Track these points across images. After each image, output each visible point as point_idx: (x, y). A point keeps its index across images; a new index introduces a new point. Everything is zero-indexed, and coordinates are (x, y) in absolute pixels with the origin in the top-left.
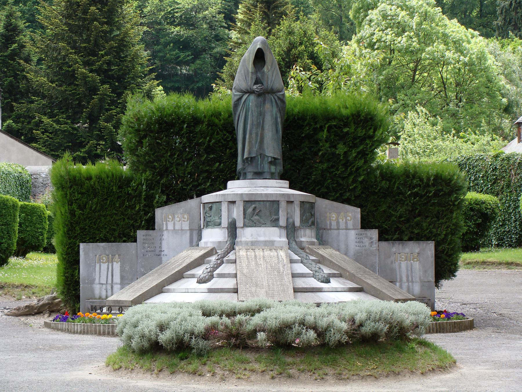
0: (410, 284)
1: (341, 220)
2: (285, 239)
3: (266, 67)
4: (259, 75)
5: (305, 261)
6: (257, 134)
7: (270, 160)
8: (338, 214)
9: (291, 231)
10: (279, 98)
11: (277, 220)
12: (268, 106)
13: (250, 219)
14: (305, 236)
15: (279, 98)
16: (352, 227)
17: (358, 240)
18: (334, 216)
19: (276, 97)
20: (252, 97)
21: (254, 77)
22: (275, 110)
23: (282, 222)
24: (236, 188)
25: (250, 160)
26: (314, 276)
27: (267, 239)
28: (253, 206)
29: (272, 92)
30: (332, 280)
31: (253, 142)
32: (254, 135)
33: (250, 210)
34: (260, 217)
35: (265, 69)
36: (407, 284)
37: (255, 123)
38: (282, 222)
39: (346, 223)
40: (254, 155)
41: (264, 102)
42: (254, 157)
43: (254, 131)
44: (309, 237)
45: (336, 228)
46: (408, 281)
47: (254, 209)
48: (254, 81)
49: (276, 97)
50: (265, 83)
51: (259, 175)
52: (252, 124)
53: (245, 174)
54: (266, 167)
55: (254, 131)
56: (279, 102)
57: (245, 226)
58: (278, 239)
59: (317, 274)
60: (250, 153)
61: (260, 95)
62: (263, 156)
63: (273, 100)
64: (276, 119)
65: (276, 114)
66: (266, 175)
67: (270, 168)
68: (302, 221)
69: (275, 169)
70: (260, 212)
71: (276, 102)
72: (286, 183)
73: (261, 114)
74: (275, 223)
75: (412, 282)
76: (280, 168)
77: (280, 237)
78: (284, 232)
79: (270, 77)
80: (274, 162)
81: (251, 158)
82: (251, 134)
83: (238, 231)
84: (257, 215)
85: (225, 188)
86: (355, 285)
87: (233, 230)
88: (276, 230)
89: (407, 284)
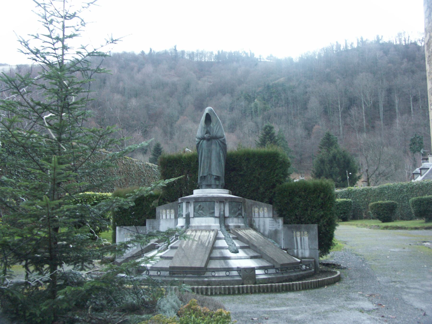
0: (303, 250)
1: (260, 212)
2: (219, 225)
3: (212, 124)
4: (208, 129)
5: (226, 238)
6: (207, 162)
7: (215, 177)
8: (259, 209)
9: (223, 219)
10: (221, 142)
11: (214, 213)
12: (214, 146)
13: (197, 213)
14: (232, 222)
15: (221, 142)
16: (267, 216)
17: (271, 224)
18: (256, 210)
19: (219, 141)
20: (205, 142)
21: (206, 130)
22: (218, 148)
23: (217, 214)
24: (197, 193)
25: (203, 178)
26: (228, 248)
27: (207, 224)
28: (199, 204)
29: (216, 138)
30: (240, 250)
31: (205, 167)
32: (206, 163)
33: (197, 207)
34: (203, 211)
35: (212, 125)
36: (301, 251)
37: (206, 156)
38: (217, 214)
39: (264, 214)
40: (205, 175)
41: (211, 144)
42: (206, 176)
43: (206, 161)
44: (236, 223)
45: (258, 217)
46: (301, 248)
47: (200, 206)
48: (205, 132)
49: (219, 141)
50: (211, 133)
51: (209, 186)
52: (205, 157)
53: (202, 186)
54: (213, 182)
55: (206, 161)
56: (221, 144)
57: (194, 217)
58: (213, 224)
59: (230, 247)
60: (203, 173)
61: (208, 140)
62: (211, 175)
63: (217, 143)
64: (219, 153)
65: (219, 151)
66: (213, 186)
67: (215, 182)
68: (230, 213)
69: (219, 183)
70: (205, 207)
71: (219, 144)
72: (227, 191)
73: (210, 151)
74: (212, 214)
75: (304, 249)
76: (223, 182)
77: (215, 223)
78: (217, 220)
79: (215, 130)
80: (218, 178)
81: (204, 176)
82: (204, 162)
83: (191, 219)
84: (201, 210)
85: (192, 194)
86: (255, 254)
87: (188, 219)
88: (212, 219)
89: (301, 251)
